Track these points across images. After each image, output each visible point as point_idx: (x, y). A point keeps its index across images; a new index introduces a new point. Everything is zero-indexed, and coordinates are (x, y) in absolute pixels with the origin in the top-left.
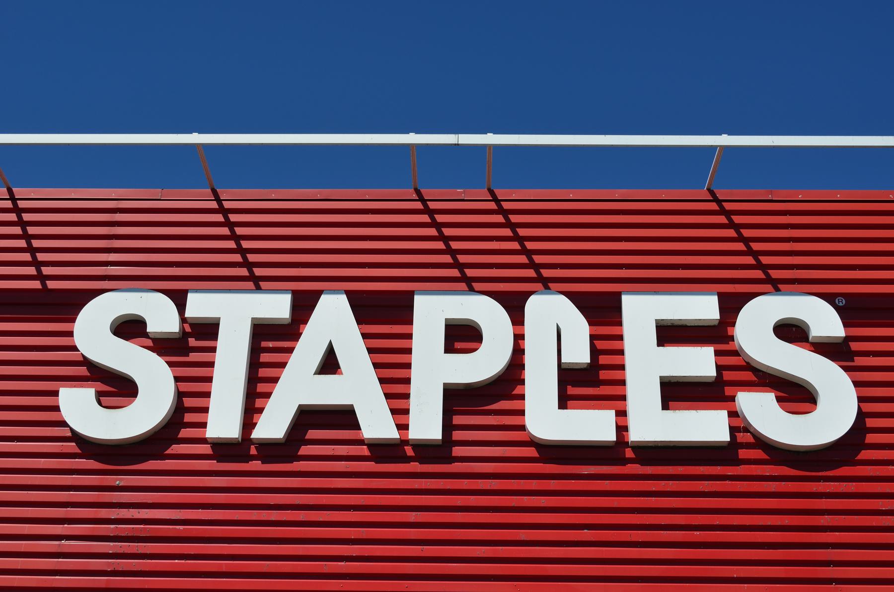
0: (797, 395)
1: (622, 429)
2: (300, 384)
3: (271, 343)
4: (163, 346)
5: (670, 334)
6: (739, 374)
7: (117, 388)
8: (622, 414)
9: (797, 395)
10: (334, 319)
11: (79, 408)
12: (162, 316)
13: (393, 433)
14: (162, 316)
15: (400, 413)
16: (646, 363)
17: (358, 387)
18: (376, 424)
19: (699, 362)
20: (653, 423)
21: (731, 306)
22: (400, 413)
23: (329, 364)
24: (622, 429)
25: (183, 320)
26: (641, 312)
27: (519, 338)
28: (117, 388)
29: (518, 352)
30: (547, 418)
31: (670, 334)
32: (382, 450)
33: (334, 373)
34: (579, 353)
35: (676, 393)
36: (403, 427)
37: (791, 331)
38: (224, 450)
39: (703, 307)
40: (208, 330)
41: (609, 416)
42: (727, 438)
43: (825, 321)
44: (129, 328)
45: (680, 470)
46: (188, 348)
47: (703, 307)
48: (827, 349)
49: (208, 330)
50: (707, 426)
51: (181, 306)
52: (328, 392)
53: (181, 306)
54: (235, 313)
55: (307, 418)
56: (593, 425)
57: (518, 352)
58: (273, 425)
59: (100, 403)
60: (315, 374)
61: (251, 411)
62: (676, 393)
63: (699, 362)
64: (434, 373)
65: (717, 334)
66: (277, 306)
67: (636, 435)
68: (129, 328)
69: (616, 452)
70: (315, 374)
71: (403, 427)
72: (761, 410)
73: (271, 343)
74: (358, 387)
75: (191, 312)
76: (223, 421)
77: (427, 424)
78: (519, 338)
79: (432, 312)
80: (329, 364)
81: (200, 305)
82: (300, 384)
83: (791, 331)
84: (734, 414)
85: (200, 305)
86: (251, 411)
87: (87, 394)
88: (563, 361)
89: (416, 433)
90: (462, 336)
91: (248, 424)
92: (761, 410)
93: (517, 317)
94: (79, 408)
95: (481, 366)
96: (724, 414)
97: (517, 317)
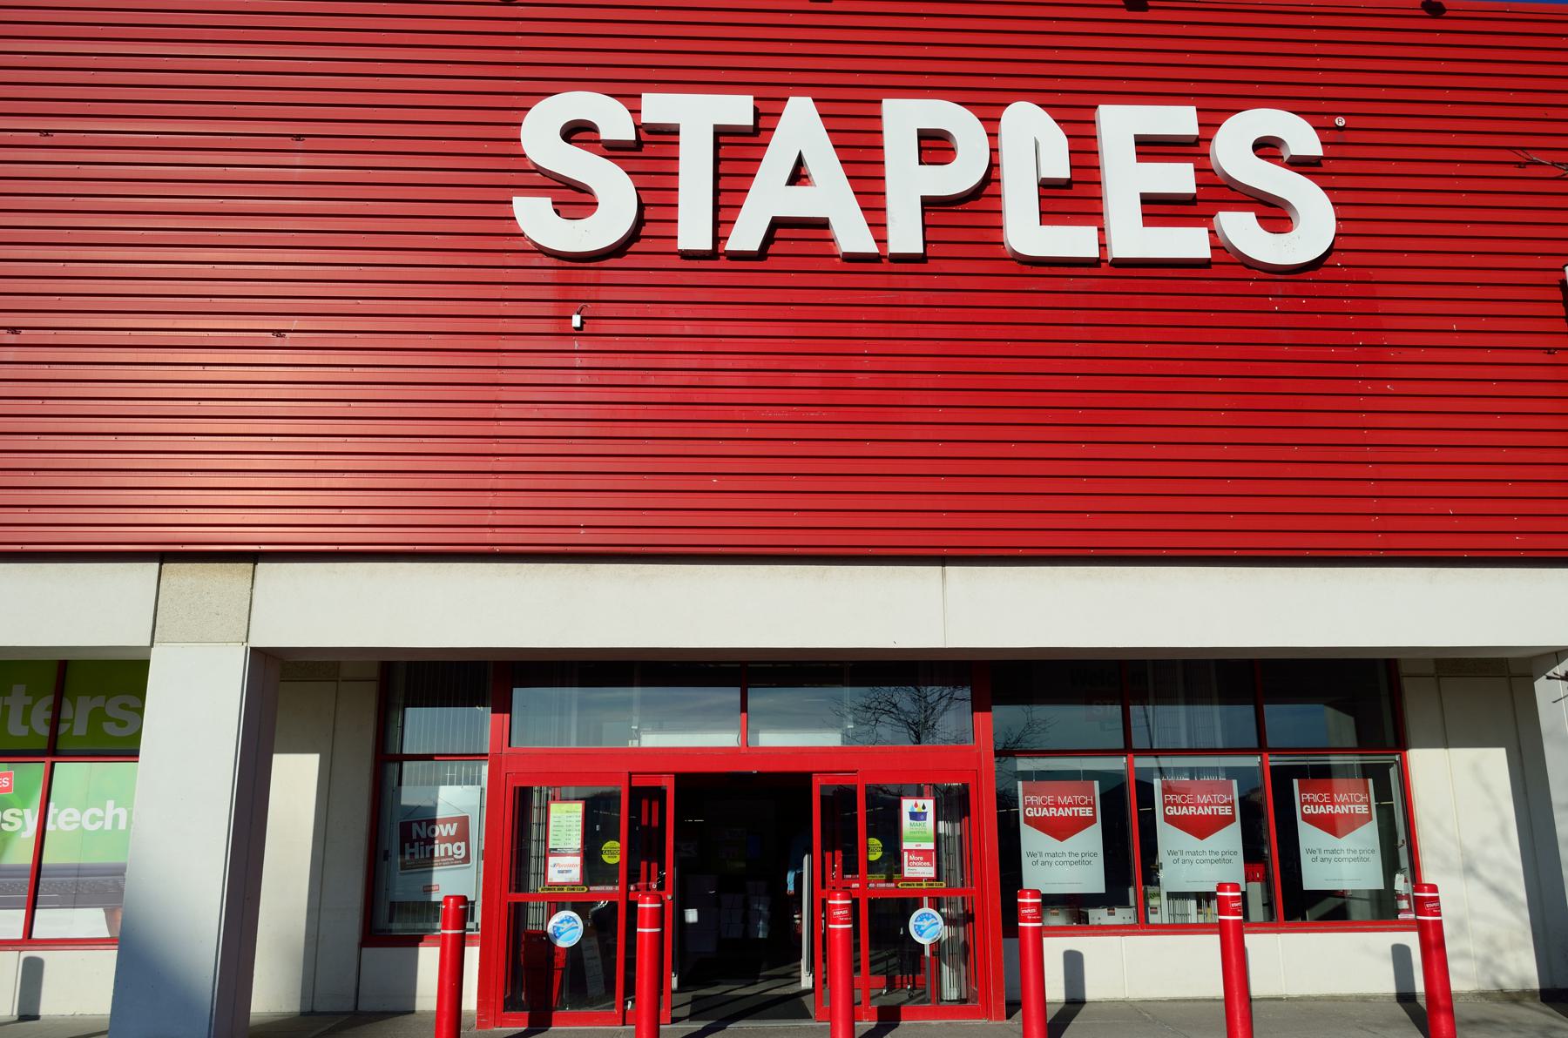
0: (1275, 214)
1: (1103, 246)
2: (768, 198)
3: (737, 153)
4: (614, 151)
5: (1151, 148)
6: (1216, 194)
7: (574, 199)
8: (1101, 230)
9: (1275, 214)
10: (801, 126)
11: (536, 218)
12: (615, 122)
13: (871, 247)
14: (615, 122)
15: (878, 226)
16: (1126, 180)
17: (831, 197)
18: (852, 236)
19: (1178, 178)
20: (1132, 238)
21: (1209, 125)
22: (878, 226)
23: (798, 176)
26: (1119, 125)
27: (994, 151)
28: (574, 199)
29: (994, 165)
30: (1026, 232)
31: (1151, 148)
33: (805, 184)
35: (1158, 209)
36: (881, 241)
37: (1267, 148)
39: (1180, 120)
40: (668, 134)
42: (633, 137)
43: (1302, 138)
44: (578, 133)
46: (650, 154)
47: (1180, 120)
48: (1301, 165)
49: (668, 134)
50: (1189, 243)
51: (635, 112)
52: (799, 203)
53: (635, 112)
54: (697, 116)
56: (1075, 241)
57: (994, 165)
58: (747, 235)
59: (557, 212)
61: (910, 851)
62: (1158, 209)
63: (1178, 178)
64: (909, 183)
66: (738, 109)
67: (1118, 251)
68: (578, 133)
71: (881, 241)
72: (1242, 230)
73: (737, 153)
74: (831, 197)
75: (647, 117)
76: (694, 232)
77: (906, 236)
78: (994, 151)
79: (903, 119)
80: (798, 176)
81: (658, 107)
82: (768, 198)
83: (1267, 148)
84: (1212, 232)
87: (545, 203)
89: (895, 247)
90: (935, 146)
91: (718, 239)
93: (991, 124)
94: (536, 218)
95: (958, 177)
96: (1205, 230)
97: (991, 124)
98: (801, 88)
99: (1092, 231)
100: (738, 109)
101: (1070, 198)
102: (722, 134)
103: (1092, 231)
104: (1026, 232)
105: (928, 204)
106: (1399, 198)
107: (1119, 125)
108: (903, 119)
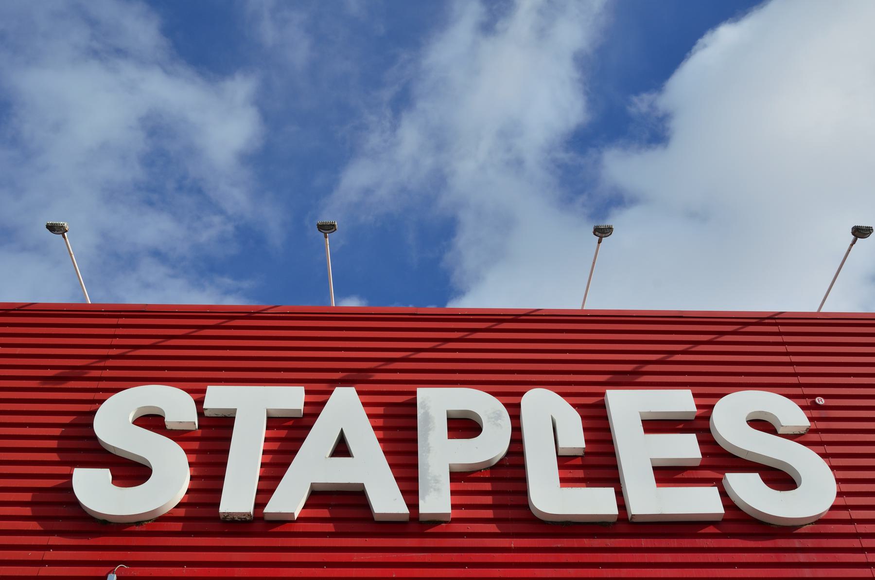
0: (780, 479)
1: (622, 504)
2: (313, 466)
3: (286, 436)
4: (178, 436)
5: (654, 425)
6: (719, 461)
7: (131, 472)
9: (780, 479)
15: (411, 493)
16: (637, 453)
18: (386, 500)
19: (685, 448)
20: (648, 499)
22: (411, 493)
23: (342, 449)
24: (622, 504)
25: (201, 413)
27: (852, 245)
28: (131, 472)
31: (654, 425)
32: (391, 526)
34: (574, 438)
35: (668, 474)
36: (413, 504)
38: (237, 525)
39: (680, 401)
41: (609, 493)
43: (790, 414)
44: (152, 421)
45: (674, 543)
46: (209, 441)
47: (680, 401)
50: (702, 501)
52: (340, 474)
53: (199, 403)
54: (252, 407)
55: (319, 496)
56: (597, 502)
60: (342, 433)
61: (265, 492)
62: (668, 474)
63: (685, 448)
65: (699, 425)
66: (291, 398)
68: (152, 421)
69: (624, 524)
70: (342, 433)
71: (413, 504)
72: (748, 489)
73: (286, 436)
76: (237, 497)
77: (436, 501)
79: (435, 403)
80: (342, 449)
81: (218, 397)
82: (313, 466)
84: (724, 494)
85: (218, 397)
86: (265, 492)
88: (560, 445)
91: (260, 504)
92: (748, 489)
94: (93, 489)
95: (490, 446)
98: (344, 383)
99: (610, 492)
100: (291, 398)
101: (594, 463)
102: (274, 422)
103: (610, 492)
104: (551, 496)
105: (456, 476)
106: (357, 557)
107: (626, 406)
108: (435, 403)
